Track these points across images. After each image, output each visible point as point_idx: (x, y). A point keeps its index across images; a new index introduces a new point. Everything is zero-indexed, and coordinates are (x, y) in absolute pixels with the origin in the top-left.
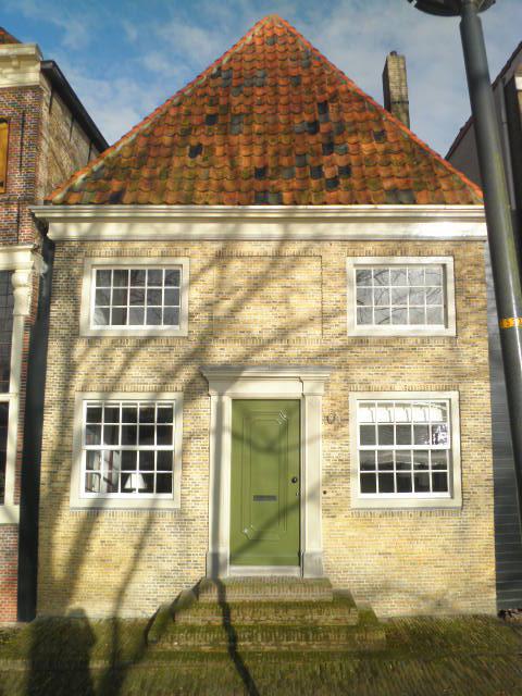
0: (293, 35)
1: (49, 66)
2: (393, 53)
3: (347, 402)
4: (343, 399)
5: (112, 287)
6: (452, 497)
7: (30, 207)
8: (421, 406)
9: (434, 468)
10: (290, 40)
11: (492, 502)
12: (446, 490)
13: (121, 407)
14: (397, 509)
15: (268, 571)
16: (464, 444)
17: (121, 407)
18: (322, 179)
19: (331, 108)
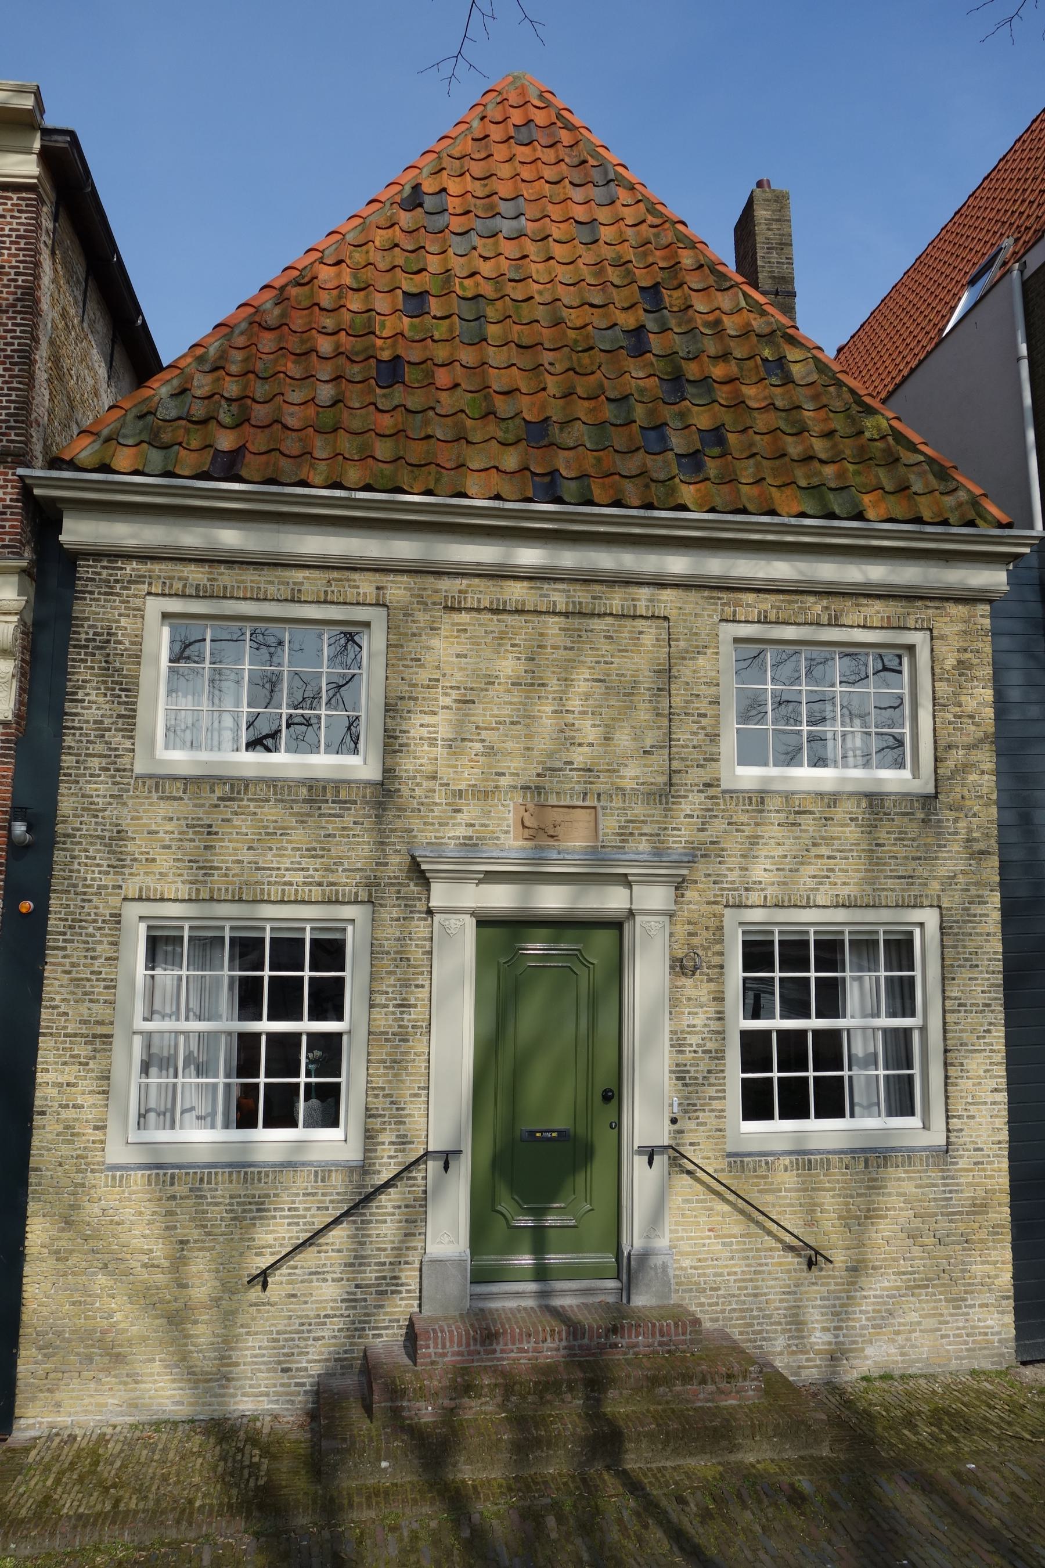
0: (570, 127)
1: (62, 141)
2: (760, 184)
3: (720, 928)
4: (712, 923)
5: (872, 690)
6: (926, 1127)
7: (21, 471)
8: (98, 1023)
9: (850, 1078)
10: (565, 137)
11: (1004, 1135)
12: (913, 1114)
13: (227, 935)
14: (819, 1152)
15: (563, 1293)
16: (951, 1018)
17: (227, 935)
18: (670, 455)
19: (671, 298)
